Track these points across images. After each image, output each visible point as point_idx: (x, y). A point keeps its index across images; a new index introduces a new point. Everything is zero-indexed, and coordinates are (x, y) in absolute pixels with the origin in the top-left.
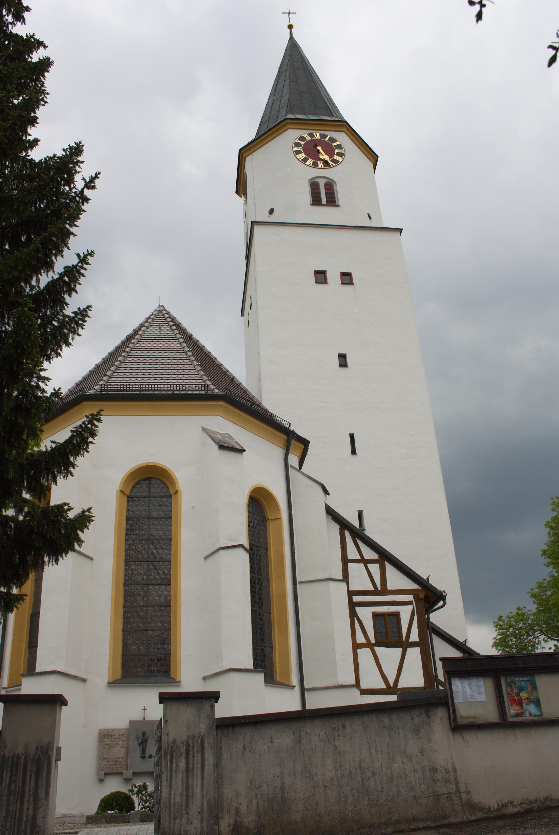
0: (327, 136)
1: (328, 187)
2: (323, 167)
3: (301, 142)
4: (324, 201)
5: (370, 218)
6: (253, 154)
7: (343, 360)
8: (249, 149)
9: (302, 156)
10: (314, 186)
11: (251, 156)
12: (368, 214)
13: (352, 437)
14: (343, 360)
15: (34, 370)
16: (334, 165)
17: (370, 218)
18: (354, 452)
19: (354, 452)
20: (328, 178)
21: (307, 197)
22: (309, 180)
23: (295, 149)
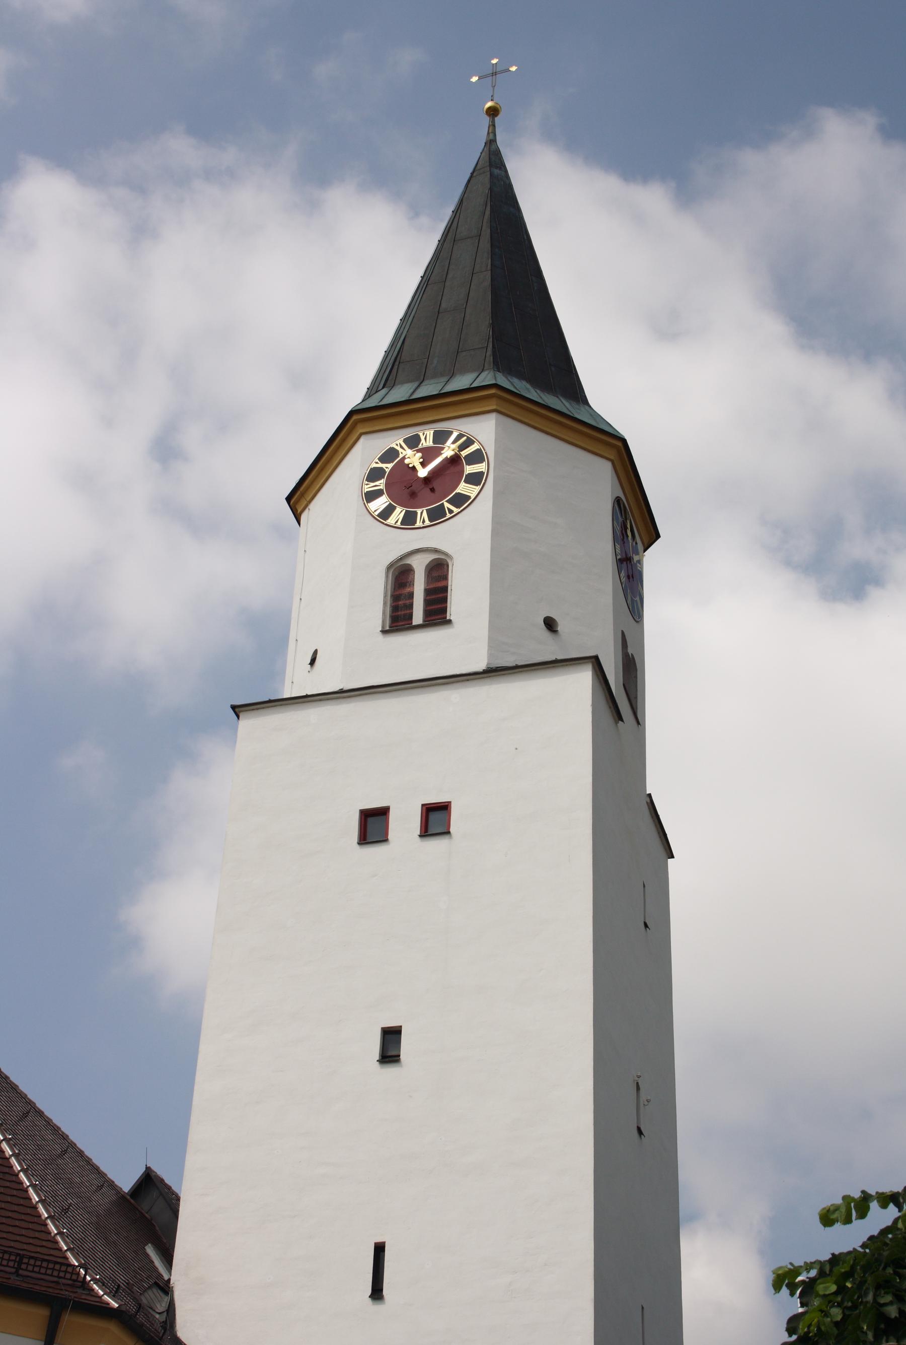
0: (451, 433)
1: (435, 574)
2: (427, 522)
3: (384, 466)
4: (418, 617)
5: (313, 662)
6: (311, 506)
7: (390, 1045)
8: (302, 495)
9: (382, 503)
10: (400, 575)
11: (307, 510)
12: (316, 652)
13: (380, 1250)
14: (390, 1045)
15: (153, 1244)
16: (456, 510)
17: (313, 662)
18: (377, 1293)
19: (377, 1293)
20: (436, 551)
21: (375, 609)
22: (389, 567)
23: (369, 487)
